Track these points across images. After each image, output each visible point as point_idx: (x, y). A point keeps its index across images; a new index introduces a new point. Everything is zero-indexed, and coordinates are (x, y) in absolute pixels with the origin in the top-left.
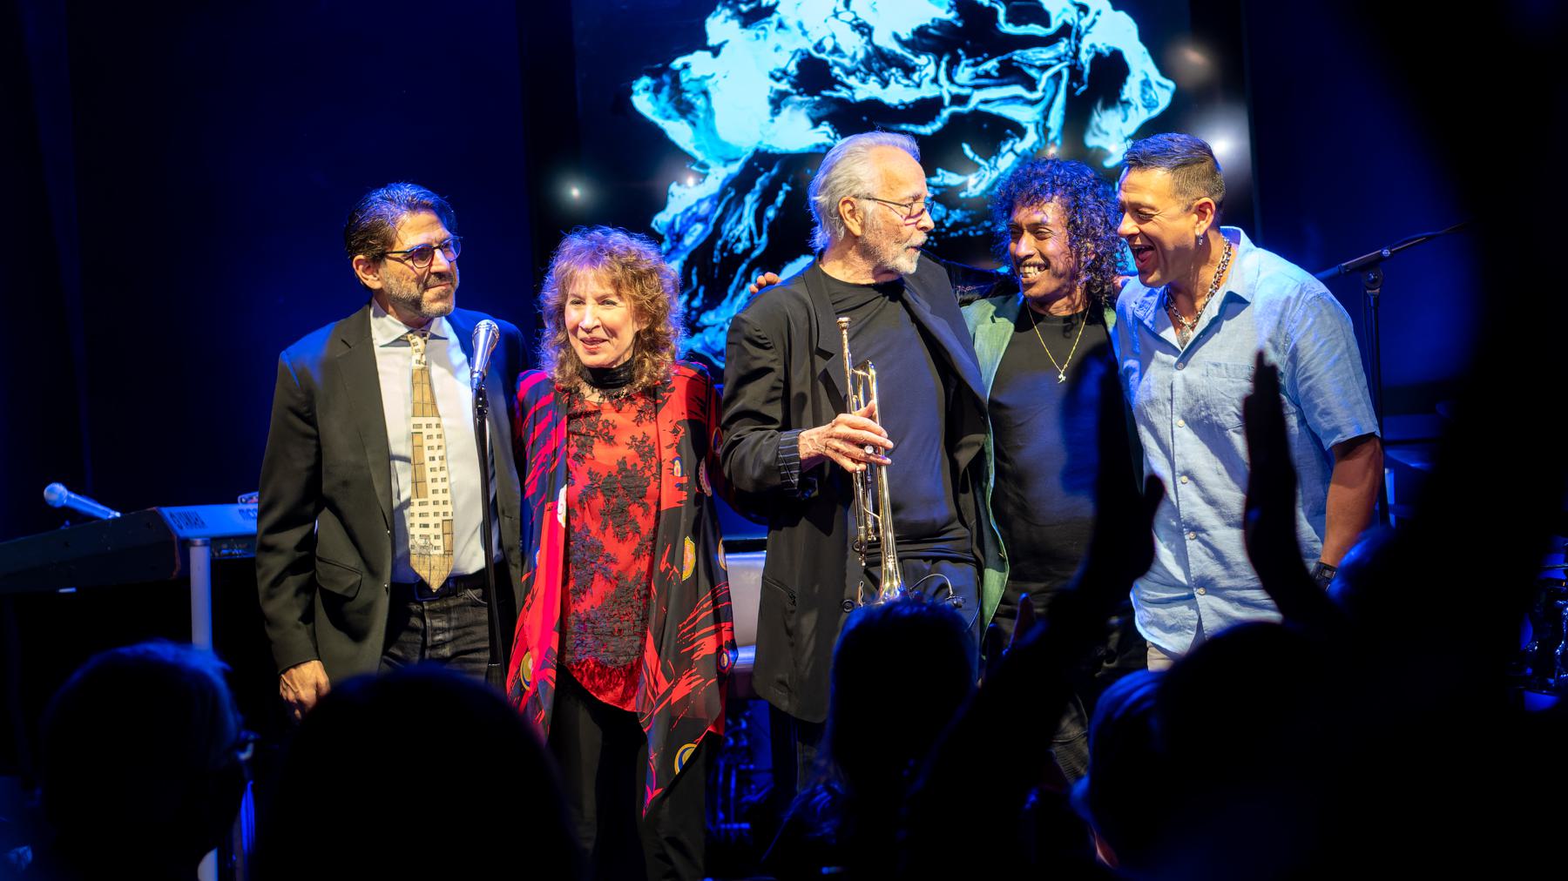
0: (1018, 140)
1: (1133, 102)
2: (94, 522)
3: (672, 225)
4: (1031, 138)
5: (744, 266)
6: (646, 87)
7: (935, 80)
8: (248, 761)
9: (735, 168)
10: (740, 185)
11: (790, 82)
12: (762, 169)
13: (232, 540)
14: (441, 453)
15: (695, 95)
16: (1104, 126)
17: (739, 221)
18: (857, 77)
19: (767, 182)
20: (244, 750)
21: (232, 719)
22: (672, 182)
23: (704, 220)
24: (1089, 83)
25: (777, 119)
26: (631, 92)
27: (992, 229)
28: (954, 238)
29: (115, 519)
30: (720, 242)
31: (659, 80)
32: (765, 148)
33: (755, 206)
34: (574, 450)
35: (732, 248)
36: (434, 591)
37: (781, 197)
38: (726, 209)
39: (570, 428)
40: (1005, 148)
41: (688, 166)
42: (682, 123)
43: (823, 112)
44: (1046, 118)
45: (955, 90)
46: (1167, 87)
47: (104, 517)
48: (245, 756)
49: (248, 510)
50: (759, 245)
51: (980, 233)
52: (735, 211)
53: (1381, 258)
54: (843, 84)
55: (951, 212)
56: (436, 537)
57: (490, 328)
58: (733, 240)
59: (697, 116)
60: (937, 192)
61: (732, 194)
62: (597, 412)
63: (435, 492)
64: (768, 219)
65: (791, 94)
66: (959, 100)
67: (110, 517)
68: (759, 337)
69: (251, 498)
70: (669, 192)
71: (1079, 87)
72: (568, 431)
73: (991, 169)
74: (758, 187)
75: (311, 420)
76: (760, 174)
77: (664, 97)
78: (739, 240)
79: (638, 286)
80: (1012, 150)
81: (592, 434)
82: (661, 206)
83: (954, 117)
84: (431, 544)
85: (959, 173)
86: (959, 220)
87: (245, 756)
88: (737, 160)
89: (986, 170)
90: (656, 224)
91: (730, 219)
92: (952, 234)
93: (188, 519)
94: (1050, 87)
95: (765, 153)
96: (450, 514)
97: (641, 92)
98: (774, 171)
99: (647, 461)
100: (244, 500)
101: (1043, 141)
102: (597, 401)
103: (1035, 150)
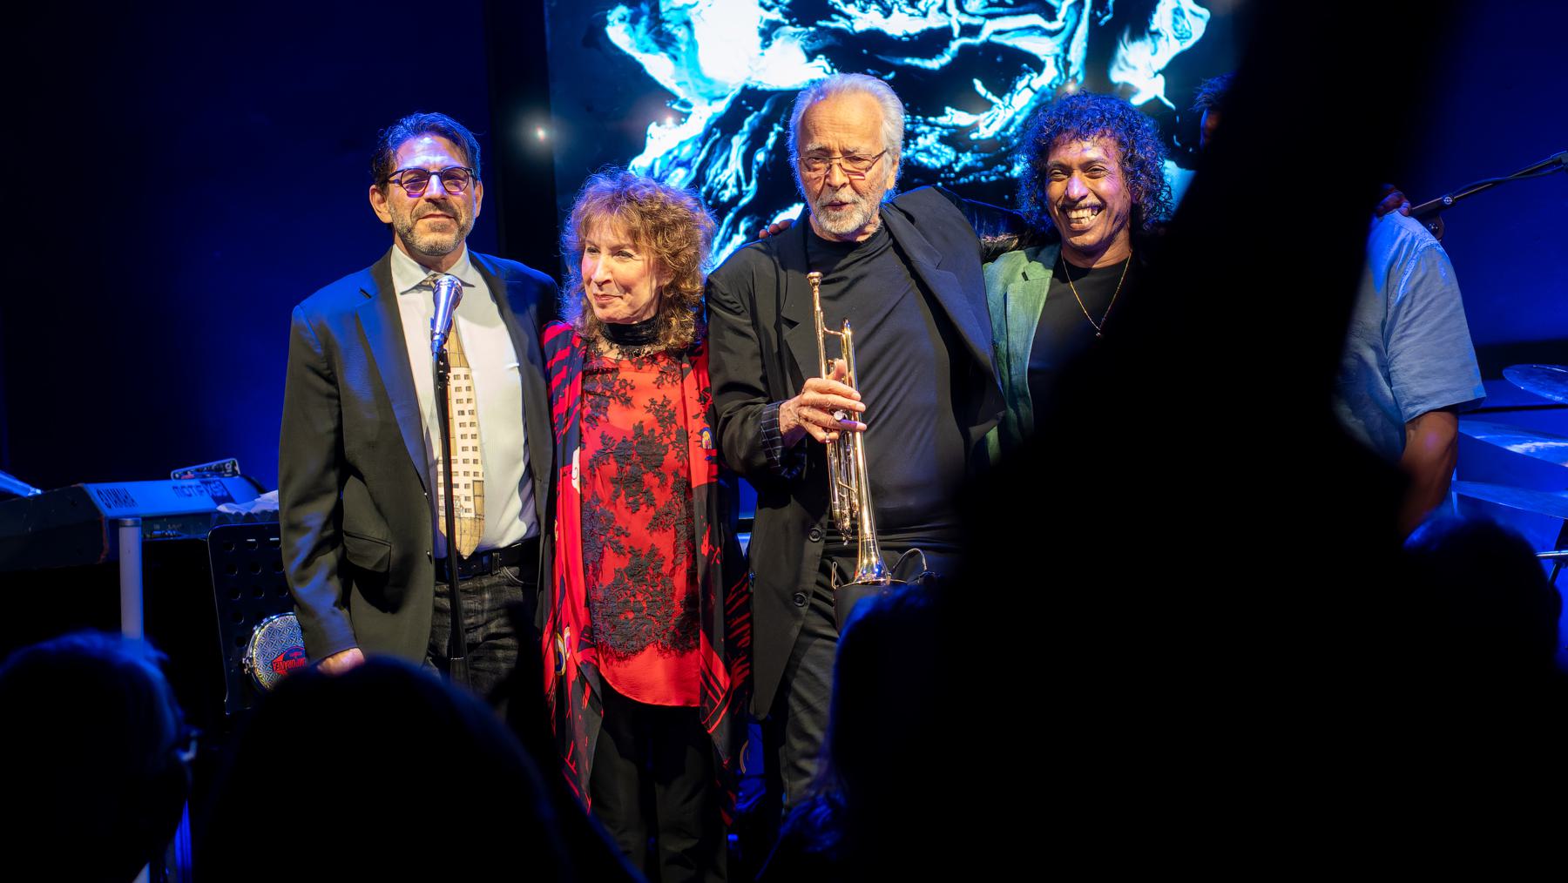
0: (1035, 74)
1: (1163, 33)
2: (14, 499)
3: (650, 171)
4: (1050, 73)
5: (731, 215)
6: (621, 17)
7: (943, 9)
8: (191, 762)
9: (721, 107)
10: (727, 124)
11: (781, 11)
12: (750, 108)
13: (165, 520)
14: (471, 407)
15: (676, 26)
16: (1130, 60)
17: (725, 165)
18: (856, 5)
19: (756, 123)
20: (187, 750)
21: (170, 716)
22: (650, 123)
23: (686, 164)
24: (1114, 13)
25: (767, 51)
26: (606, 23)
27: (1007, 174)
28: (965, 183)
29: (36, 497)
30: (704, 189)
31: (637, 10)
32: (755, 85)
33: (743, 149)
34: (588, 410)
35: (717, 195)
36: (465, 558)
37: (771, 140)
38: (710, 153)
39: (584, 387)
40: (1021, 84)
41: (668, 105)
42: (662, 57)
43: (819, 44)
44: (1066, 51)
45: (965, 20)
46: (1201, 16)
47: (24, 494)
48: (187, 756)
49: (183, 487)
50: (748, 192)
51: (993, 178)
52: (721, 154)
53: (1442, 205)
54: (840, 13)
55: (960, 155)
56: (467, 499)
57: (453, 284)
58: (719, 187)
59: (678, 49)
60: (945, 133)
61: (718, 135)
62: (615, 370)
63: (464, 449)
64: (758, 163)
65: (784, 25)
66: (973, 31)
67: (30, 494)
68: (728, 301)
69: (186, 473)
70: (648, 133)
71: (1103, 16)
72: (582, 390)
73: (1005, 107)
74: (746, 128)
75: (331, 379)
76: (750, 113)
77: (642, 27)
78: (725, 186)
79: (659, 238)
80: (1028, 86)
81: (608, 394)
82: (639, 148)
83: (964, 49)
84: (461, 506)
85: (970, 112)
86: (969, 164)
87: (187, 756)
88: (723, 97)
89: (1000, 108)
90: (634, 169)
91: (716, 163)
92: (962, 180)
93: (117, 497)
94: (1071, 16)
95: (754, 90)
96: (480, 474)
97: (616, 22)
98: (764, 110)
99: (666, 427)
100: (177, 476)
101: (1064, 76)
102: (615, 357)
103: (1054, 86)
